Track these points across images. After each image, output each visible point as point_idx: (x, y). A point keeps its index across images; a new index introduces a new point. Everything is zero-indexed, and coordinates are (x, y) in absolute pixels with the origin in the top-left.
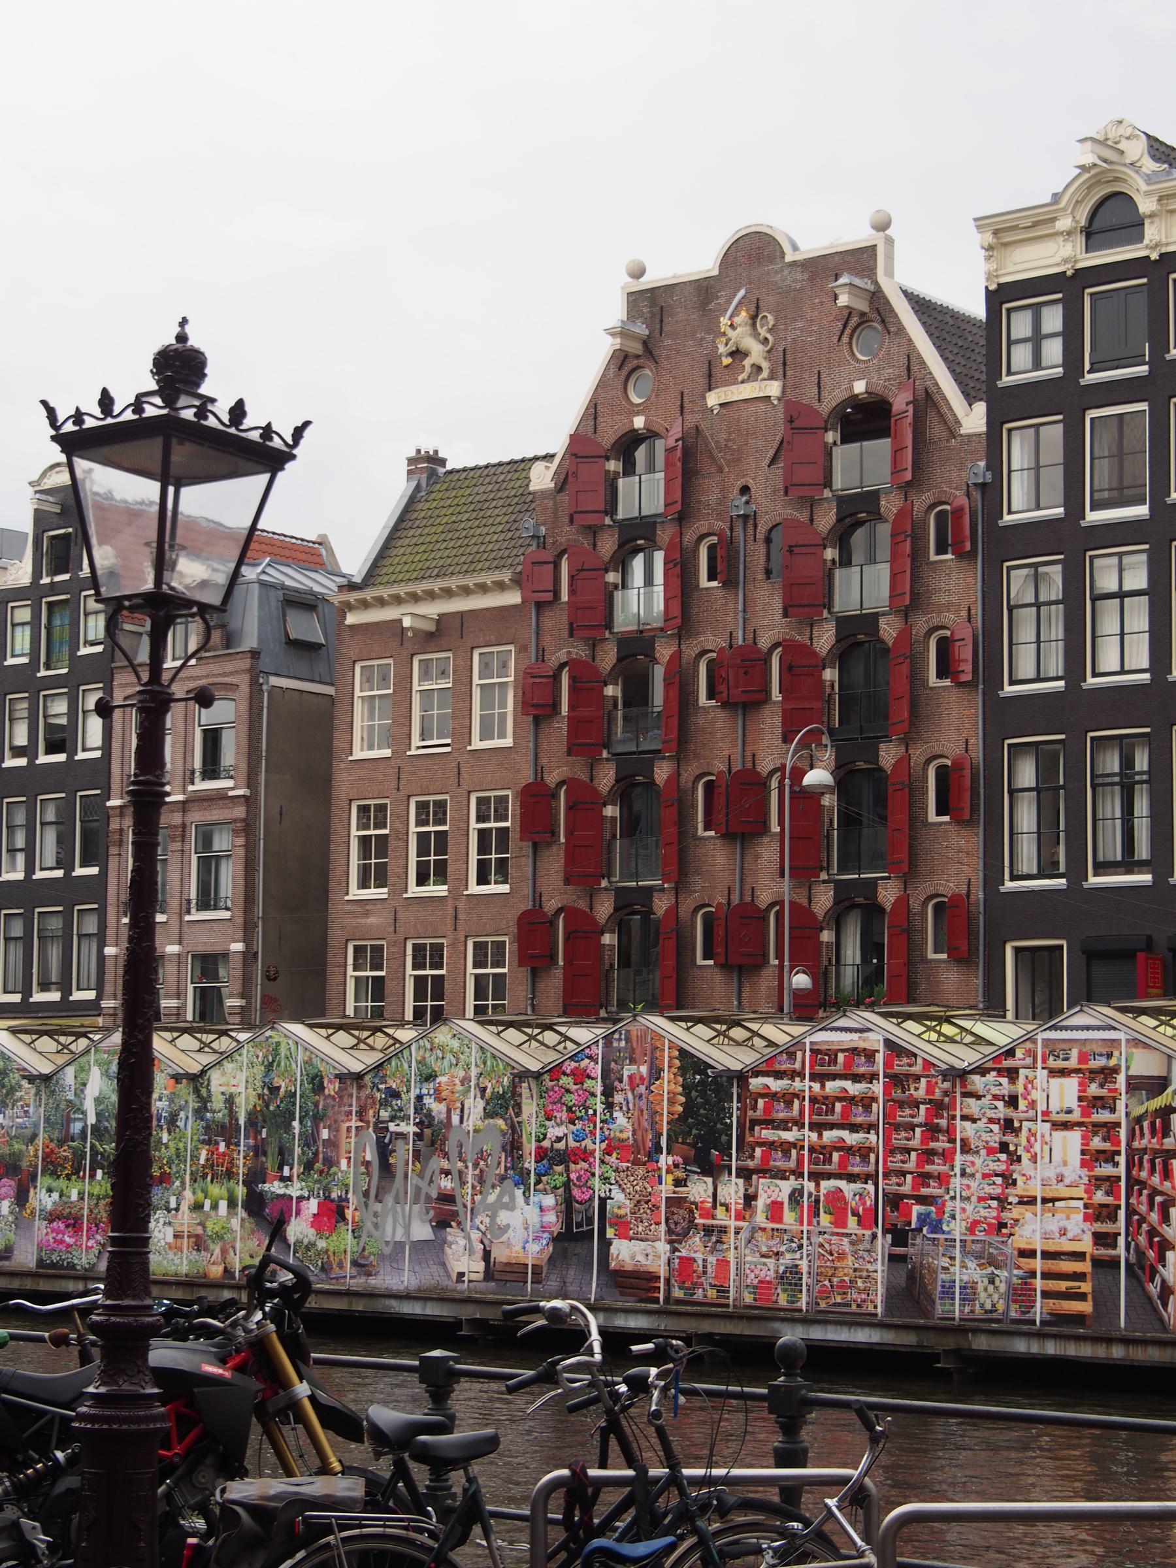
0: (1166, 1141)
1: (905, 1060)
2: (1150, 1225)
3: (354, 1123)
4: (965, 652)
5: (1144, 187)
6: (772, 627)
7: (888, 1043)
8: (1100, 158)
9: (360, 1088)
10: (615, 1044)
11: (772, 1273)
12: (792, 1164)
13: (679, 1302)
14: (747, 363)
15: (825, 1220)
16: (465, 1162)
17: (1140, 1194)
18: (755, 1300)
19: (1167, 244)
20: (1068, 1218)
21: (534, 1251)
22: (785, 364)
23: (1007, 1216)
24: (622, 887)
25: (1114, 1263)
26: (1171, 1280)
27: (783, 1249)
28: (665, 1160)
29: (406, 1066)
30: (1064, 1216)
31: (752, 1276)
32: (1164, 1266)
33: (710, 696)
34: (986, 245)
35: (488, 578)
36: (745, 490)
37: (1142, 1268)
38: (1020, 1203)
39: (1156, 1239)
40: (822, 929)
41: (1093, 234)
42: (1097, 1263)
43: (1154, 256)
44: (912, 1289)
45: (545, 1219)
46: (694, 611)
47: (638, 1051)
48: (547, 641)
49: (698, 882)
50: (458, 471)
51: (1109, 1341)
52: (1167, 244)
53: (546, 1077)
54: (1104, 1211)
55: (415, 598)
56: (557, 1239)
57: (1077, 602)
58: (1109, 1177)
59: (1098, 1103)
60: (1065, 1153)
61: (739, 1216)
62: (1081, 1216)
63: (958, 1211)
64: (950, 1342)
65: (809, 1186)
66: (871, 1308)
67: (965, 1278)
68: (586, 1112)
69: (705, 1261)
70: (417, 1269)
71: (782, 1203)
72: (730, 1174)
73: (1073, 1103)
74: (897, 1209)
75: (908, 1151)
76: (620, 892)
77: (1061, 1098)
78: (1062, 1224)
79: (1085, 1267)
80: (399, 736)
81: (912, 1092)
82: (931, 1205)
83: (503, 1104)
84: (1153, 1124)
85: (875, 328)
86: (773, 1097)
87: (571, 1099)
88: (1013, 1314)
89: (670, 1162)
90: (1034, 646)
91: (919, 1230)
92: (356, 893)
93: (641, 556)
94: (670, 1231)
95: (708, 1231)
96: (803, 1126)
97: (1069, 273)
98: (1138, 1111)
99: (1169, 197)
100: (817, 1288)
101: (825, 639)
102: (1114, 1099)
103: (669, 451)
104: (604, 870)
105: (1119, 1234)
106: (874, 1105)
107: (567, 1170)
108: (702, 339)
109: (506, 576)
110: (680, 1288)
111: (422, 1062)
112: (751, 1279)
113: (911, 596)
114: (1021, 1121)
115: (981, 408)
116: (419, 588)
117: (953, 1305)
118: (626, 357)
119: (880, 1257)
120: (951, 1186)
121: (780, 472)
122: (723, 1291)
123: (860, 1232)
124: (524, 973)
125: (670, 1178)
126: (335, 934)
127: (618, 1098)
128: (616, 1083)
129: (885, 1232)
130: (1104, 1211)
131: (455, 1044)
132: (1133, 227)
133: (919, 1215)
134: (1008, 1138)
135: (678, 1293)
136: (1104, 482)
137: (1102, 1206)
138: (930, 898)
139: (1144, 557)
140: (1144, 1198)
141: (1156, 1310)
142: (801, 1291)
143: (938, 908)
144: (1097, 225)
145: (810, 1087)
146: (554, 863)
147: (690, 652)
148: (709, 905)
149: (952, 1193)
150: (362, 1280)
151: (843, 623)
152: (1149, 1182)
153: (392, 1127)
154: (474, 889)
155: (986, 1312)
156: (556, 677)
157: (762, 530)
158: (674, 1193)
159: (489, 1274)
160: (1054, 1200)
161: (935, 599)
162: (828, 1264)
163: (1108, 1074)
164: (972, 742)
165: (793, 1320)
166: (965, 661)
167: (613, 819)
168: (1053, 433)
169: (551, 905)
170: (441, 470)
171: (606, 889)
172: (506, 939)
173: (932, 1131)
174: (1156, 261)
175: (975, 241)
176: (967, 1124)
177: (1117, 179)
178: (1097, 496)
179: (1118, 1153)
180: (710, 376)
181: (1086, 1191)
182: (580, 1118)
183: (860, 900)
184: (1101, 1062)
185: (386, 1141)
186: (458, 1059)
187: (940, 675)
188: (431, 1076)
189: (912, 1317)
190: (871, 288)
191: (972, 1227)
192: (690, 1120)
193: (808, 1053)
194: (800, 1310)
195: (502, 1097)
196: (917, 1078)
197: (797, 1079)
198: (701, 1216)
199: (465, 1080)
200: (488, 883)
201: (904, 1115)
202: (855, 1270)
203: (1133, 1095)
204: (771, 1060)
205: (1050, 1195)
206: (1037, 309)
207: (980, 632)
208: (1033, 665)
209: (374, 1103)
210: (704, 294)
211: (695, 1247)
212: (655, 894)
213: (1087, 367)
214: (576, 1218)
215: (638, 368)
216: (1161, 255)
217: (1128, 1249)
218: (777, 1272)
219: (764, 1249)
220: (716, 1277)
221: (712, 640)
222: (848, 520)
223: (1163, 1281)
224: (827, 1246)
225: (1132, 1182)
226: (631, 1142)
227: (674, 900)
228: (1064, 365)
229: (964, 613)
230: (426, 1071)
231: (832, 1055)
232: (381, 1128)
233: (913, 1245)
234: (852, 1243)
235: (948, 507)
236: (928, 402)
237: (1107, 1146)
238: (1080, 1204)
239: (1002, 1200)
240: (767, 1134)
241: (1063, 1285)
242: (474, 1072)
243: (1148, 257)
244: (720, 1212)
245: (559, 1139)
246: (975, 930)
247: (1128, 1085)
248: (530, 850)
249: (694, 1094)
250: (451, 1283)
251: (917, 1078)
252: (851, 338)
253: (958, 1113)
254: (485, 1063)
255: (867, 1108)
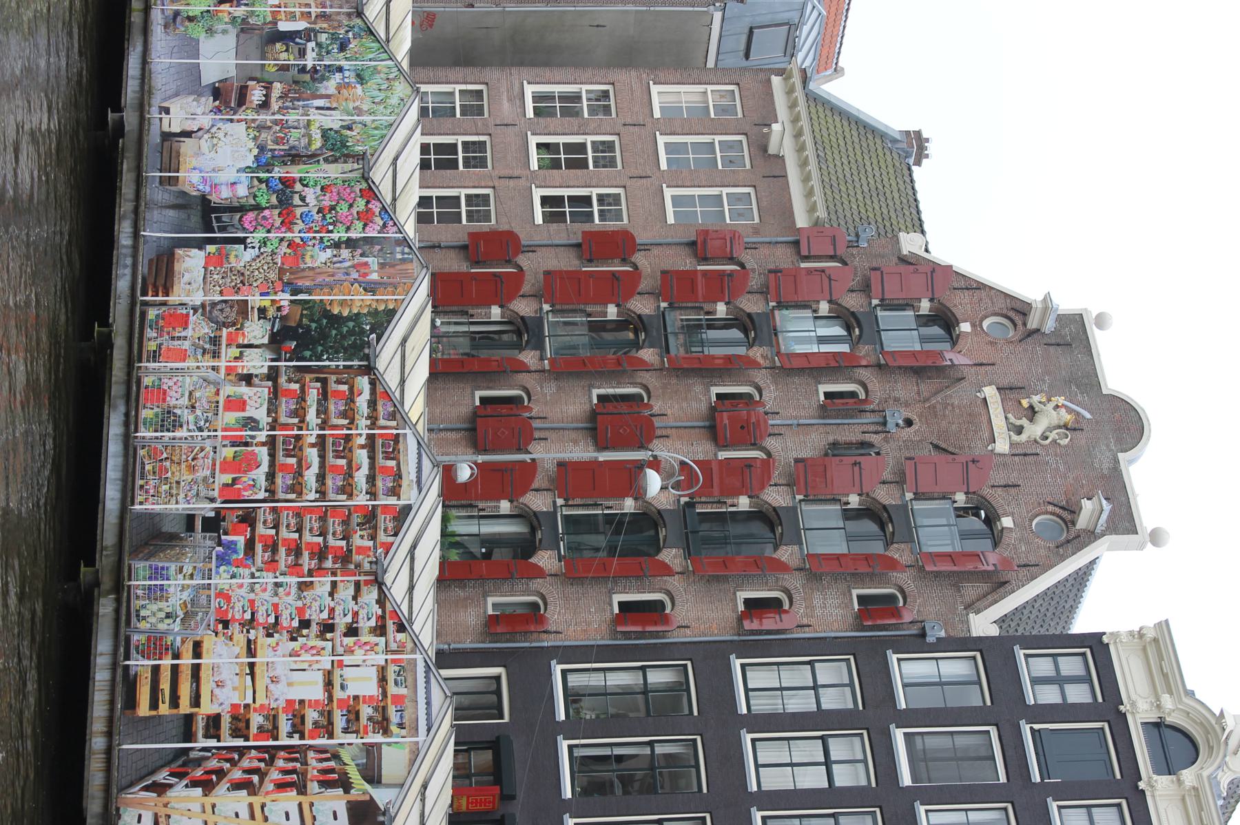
0: (316, 784)
1: (390, 525)
2: (229, 771)
3: (314, 10)
4: (769, 623)
5: (1205, 774)
6: (789, 447)
7: (407, 509)
8: (1231, 732)
9: (349, 15)
10: (398, 249)
11: (174, 402)
12: (283, 419)
13: (143, 315)
14: (1024, 422)
15: (229, 452)
16: (278, 112)
17: (260, 760)
18: (147, 387)
19: (1153, 796)
20: (235, 689)
21: (191, 178)
22: (1025, 455)
23: (235, 628)
24: (548, 310)
25: (189, 736)
26: (171, 794)
27: (199, 412)
28: (285, 298)
29: (371, 56)
30: (237, 684)
31: (171, 383)
32: (187, 786)
33: (719, 396)
34: (1144, 631)
35: (818, 197)
36: (909, 423)
37: (184, 764)
38: (249, 641)
39: (214, 777)
40: (511, 501)
41: (1157, 728)
42: (189, 719)
43: (1142, 785)
44: (157, 538)
45: (223, 188)
46: (796, 380)
47: (392, 270)
48: (764, 251)
49: (550, 388)
50: (911, 175)
51: (109, 734)
52: (1153, 796)
53: (364, 185)
54: (242, 725)
55: (798, 135)
56: (204, 200)
57: (820, 722)
58: (277, 728)
59: (353, 715)
60: (302, 683)
61: (229, 370)
62: (236, 701)
63: (240, 581)
64: (107, 582)
65: (262, 436)
66: (139, 499)
67: (172, 590)
68: (330, 224)
69: (185, 338)
70: (172, 70)
71: (244, 410)
72: (273, 360)
73: (352, 691)
74: (240, 522)
75: (299, 530)
76: (539, 321)
77: (354, 679)
78: (229, 683)
79: (185, 707)
80: (673, 122)
81: (359, 533)
82: (246, 554)
83: (337, 147)
84: (332, 771)
85: (1061, 535)
86: (351, 399)
87: (343, 208)
88: (135, 638)
89: (282, 303)
90: (778, 686)
91: (220, 544)
92: (529, 90)
93: (842, 332)
94: (214, 304)
95: (215, 341)
96: (322, 429)
97: (1121, 708)
98: (345, 755)
99: (1198, 796)
100: (160, 447)
101: (776, 497)
102: (357, 732)
103: (940, 354)
104: (558, 307)
105: (219, 741)
106: (345, 497)
107: (273, 207)
108: (1044, 381)
109: (821, 213)
110: (157, 316)
111: (376, 70)
112: (167, 383)
113: (819, 570)
114: (332, 640)
115: (994, 631)
116: (807, 138)
117: (145, 579)
118: (1025, 314)
119: (191, 506)
120: (264, 574)
121: (926, 452)
122: (155, 356)
123: (216, 486)
124: (464, 239)
125: (267, 304)
126: (492, 74)
127: (345, 253)
128: (359, 251)
129: (217, 511)
130: (242, 725)
131: (394, 101)
132: (1167, 766)
133: (235, 543)
134: (314, 628)
135: (152, 313)
136: (931, 742)
137: (248, 722)
138: (543, 598)
139: (864, 783)
140: (256, 764)
141: (142, 779)
142: (156, 431)
143: (535, 606)
144: (1168, 733)
145: (361, 435)
146: (567, 262)
147: (761, 377)
148: (529, 400)
149: (257, 574)
150: (161, 21)
151: (792, 510)
152: (273, 769)
153: (311, 45)
154: (537, 194)
155: (138, 611)
156: (731, 260)
157: (874, 439)
158: (252, 308)
159: (167, 136)
160: (252, 674)
161: (817, 595)
162: (184, 457)
163: (383, 725)
164: (688, 631)
165: (126, 424)
166: (761, 624)
167: (605, 314)
168: (976, 698)
169: (524, 260)
170: (911, 161)
171: (541, 309)
172: (493, 222)
173: (320, 553)
174: (1137, 787)
175: (1149, 621)
176: (328, 588)
177: (1211, 748)
178: (918, 740)
179: (302, 737)
180: (1011, 389)
181: (262, 706)
182: (324, 218)
183: (539, 535)
184: (394, 718)
185: (298, 40)
186: (379, 103)
187: (747, 602)
188: (362, 79)
189: (131, 539)
190: (1098, 531)
191: (224, 595)
192: (325, 321)
193: (395, 432)
194: (136, 431)
195: (344, 145)
196: (373, 537)
197: (369, 422)
198: (229, 334)
199: (359, 111)
200: (543, 205)
201: (334, 525)
202: (178, 483)
203: (361, 750)
204: (387, 395)
205: (257, 670)
206: (1087, 679)
207: (788, 636)
208: (760, 684)
209: (335, 28)
210: (1084, 379)
211: (199, 328)
212: (538, 352)
213: (1036, 727)
214: (225, 217)
215: (1015, 325)
216: (1143, 791)
217: (204, 749)
218: (175, 407)
219: (198, 394)
220: (169, 349)
221: (771, 396)
222: (885, 515)
223: (171, 786)
224: (202, 455)
225: (272, 752)
226: (302, 266)
227: (533, 369)
228: (1036, 705)
229: (805, 621)
230: (366, 75)
231: (393, 455)
232: (308, 34)
233: (205, 538)
234: (205, 479)
235: (901, 604)
236: (998, 585)
237: (309, 725)
238: (249, 700)
239: (251, 623)
240: (313, 395)
241: (165, 685)
242: (367, 118)
243: (1140, 779)
244: (235, 352)
245: (303, 199)
246: (515, 643)
247: (372, 745)
248: (574, 241)
249: (351, 324)
250: (156, 101)
251: (373, 537)
252: (1051, 513)
253: (338, 579)
254: (376, 128)
255: (342, 490)
